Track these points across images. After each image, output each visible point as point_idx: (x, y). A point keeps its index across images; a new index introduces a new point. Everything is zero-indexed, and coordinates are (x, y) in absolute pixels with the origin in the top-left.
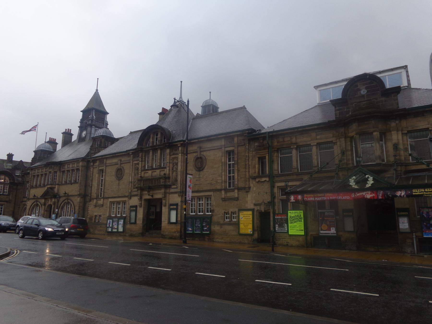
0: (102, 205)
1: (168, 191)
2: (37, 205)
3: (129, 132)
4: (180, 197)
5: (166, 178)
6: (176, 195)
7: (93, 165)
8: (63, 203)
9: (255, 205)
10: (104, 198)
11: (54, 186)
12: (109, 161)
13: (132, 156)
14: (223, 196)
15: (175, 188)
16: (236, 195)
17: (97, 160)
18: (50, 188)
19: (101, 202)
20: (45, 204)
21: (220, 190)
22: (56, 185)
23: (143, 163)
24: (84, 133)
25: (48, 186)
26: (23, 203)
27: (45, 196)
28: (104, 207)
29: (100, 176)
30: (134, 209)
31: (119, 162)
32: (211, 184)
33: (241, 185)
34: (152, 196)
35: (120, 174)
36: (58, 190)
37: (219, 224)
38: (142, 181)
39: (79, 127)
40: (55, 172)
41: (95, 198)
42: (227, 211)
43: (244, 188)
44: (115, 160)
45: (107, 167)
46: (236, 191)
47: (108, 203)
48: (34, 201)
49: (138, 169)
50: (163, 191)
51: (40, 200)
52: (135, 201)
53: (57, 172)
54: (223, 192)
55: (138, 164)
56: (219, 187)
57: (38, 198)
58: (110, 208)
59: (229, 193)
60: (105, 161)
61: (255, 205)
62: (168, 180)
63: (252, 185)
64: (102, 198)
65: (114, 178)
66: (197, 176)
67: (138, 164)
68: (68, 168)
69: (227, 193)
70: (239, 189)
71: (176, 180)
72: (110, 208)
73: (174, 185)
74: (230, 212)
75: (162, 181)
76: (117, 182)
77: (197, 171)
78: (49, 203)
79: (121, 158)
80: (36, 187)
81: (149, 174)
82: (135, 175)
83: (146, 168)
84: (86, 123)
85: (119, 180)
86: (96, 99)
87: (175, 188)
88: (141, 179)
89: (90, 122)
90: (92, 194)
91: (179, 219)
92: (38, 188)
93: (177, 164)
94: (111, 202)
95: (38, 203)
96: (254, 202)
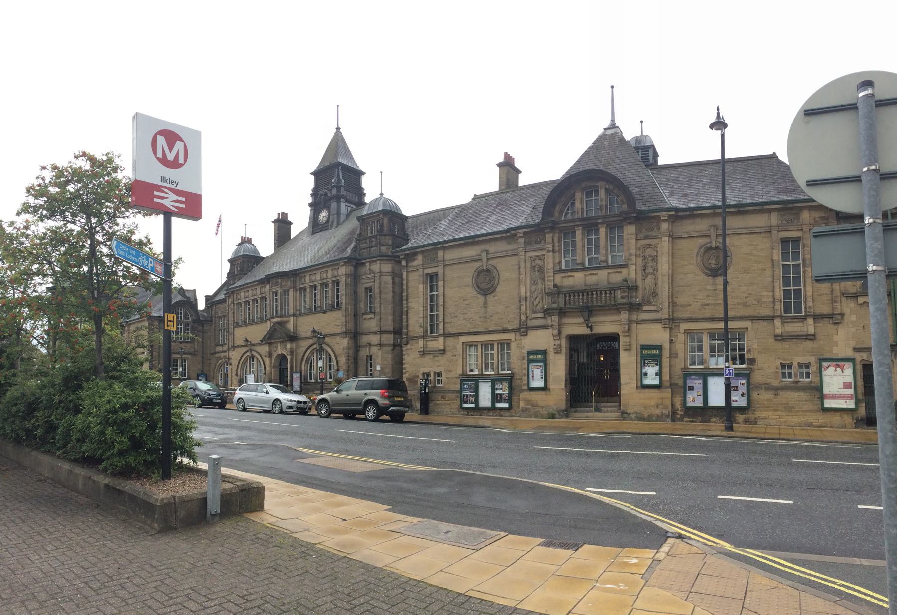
0: (443, 351)
1: (634, 317)
2: (253, 357)
3: (473, 196)
4: (668, 330)
5: (630, 288)
6: (658, 327)
7: (407, 266)
8: (309, 351)
9: (856, 349)
10: (445, 335)
11: (285, 319)
12: (451, 255)
13: (522, 240)
14: (779, 331)
15: (652, 311)
16: (811, 330)
17: (416, 254)
18: (278, 323)
19: (439, 343)
20: (270, 355)
21: (772, 318)
22: (289, 316)
23: (557, 255)
24: (324, 215)
25: (275, 320)
26: (217, 355)
27: (269, 339)
28: (448, 355)
29: (426, 288)
30: (541, 356)
31: (484, 255)
32: (745, 305)
33: (825, 309)
34: (591, 328)
35: (486, 283)
36: (295, 326)
37: (768, 387)
38: (561, 296)
39: (310, 205)
40: (286, 292)
41: (421, 337)
42: (788, 362)
43: (831, 316)
44: (469, 252)
45: (447, 269)
46: (810, 321)
47: (460, 347)
48: (244, 349)
49: (541, 270)
50: (625, 315)
51: (258, 348)
52: (540, 339)
53: (288, 291)
54: (778, 322)
55: (541, 258)
56: (768, 312)
57: (252, 345)
58: (464, 358)
59: (790, 325)
60: (440, 253)
61: (856, 349)
62: (634, 294)
63: (846, 311)
64: (440, 335)
65: (471, 292)
66: (709, 287)
67: (541, 258)
68: (311, 281)
69: (786, 324)
70: (817, 317)
71: (655, 294)
72: (464, 358)
73: (649, 303)
74: (795, 364)
75: (619, 294)
76: (481, 299)
77: (707, 275)
78: (279, 351)
79: (486, 247)
80: (245, 324)
81: (577, 279)
82: (534, 283)
83: (563, 267)
84: (326, 194)
85: (485, 295)
86: (338, 144)
87: (652, 311)
88: (558, 290)
89: (334, 192)
90: (410, 329)
91: (666, 377)
92: (249, 324)
93: (655, 259)
94: (469, 345)
95: (254, 353)
96: (853, 343)
